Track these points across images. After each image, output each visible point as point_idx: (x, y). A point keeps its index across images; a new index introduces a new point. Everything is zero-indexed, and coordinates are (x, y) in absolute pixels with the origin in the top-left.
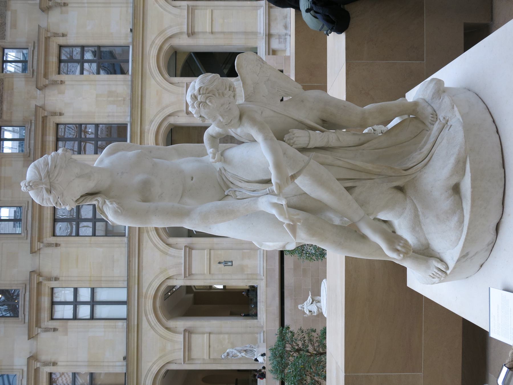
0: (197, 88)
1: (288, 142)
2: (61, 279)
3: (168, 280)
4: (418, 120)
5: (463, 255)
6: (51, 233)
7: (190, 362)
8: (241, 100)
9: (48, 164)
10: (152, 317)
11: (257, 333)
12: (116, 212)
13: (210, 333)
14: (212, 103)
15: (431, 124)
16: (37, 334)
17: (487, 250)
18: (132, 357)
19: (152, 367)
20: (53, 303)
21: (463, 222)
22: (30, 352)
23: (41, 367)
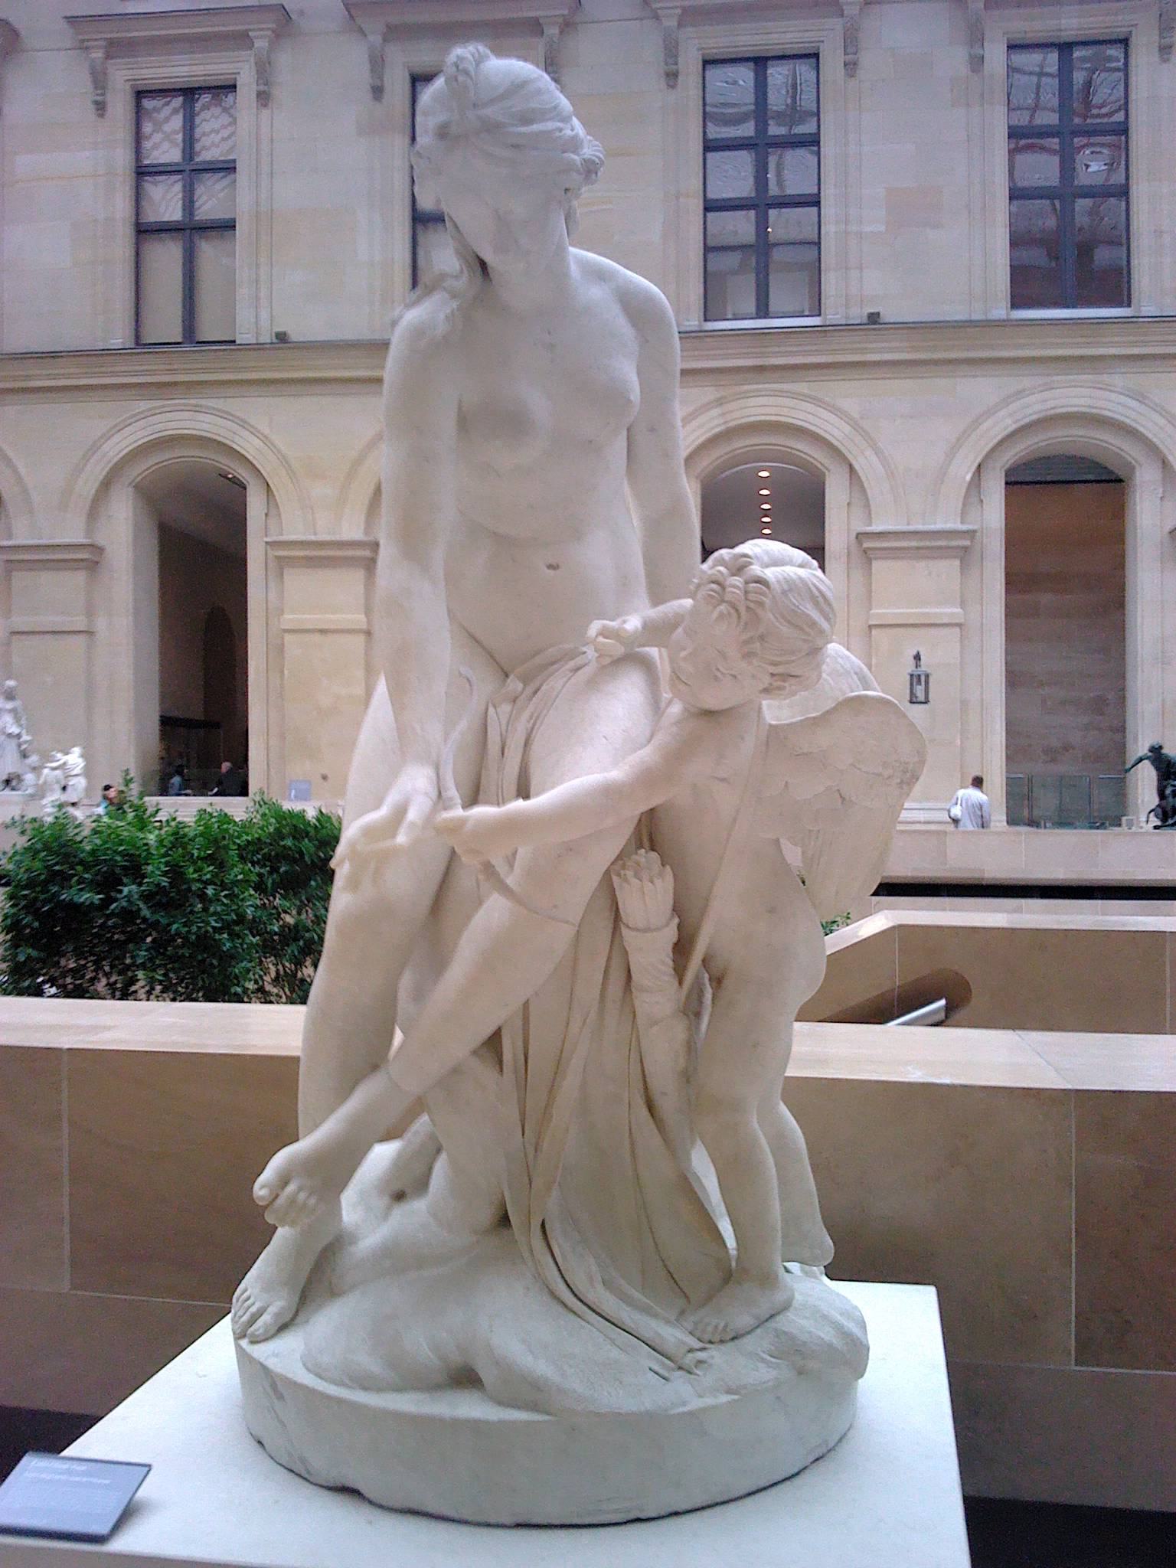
0: (770, 574)
4: (710, 1284)
6: (714, 53)
8: (776, 712)
12: (418, 332)
13: (368, 633)
17: (290, 1455)
19: (255, 432)
21: (365, 1389)
22: (302, 13)
23: (252, 52)
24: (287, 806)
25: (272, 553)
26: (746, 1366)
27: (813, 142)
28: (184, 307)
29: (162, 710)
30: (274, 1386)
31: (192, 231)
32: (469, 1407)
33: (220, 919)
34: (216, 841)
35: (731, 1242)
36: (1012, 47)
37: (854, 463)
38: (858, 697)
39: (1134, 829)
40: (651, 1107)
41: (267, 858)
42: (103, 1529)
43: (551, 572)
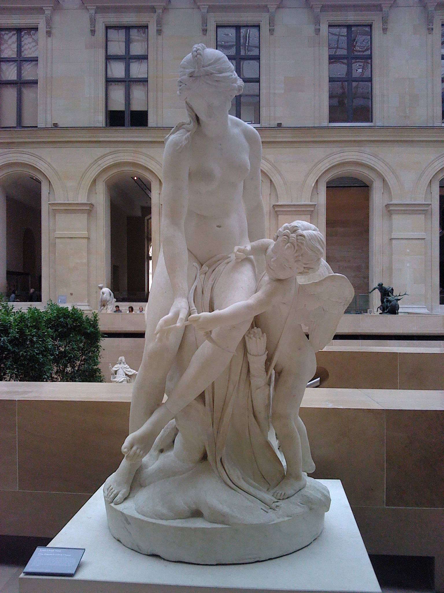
0: (305, 233)
1: (251, 332)
2: (160, 37)
3: (158, 182)
5: (129, 519)
6: (220, 23)
7: (51, 211)
8: (301, 280)
9: (221, 73)
10: (109, 161)
11: (88, 302)
12: (176, 144)
13: (88, 238)
14: (287, 249)
15: (274, 493)
16: (87, 9)
18: (58, 135)
20: (128, 28)
21: (162, 519)
24: (61, 305)
25: (51, 208)
26: (293, 507)
27: (257, 58)
28: (17, 113)
29: (7, 268)
30: (126, 520)
31: (21, 84)
32: (199, 524)
33: (38, 350)
34: (36, 318)
35: (284, 463)
36: (330, 26)
37: (272, 179)
38: (333, 276)
39: (372, 314)
40: (255, 416)
41: (53, 326)
42: (73, 572)
43: (218, 228)
